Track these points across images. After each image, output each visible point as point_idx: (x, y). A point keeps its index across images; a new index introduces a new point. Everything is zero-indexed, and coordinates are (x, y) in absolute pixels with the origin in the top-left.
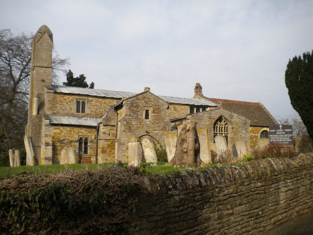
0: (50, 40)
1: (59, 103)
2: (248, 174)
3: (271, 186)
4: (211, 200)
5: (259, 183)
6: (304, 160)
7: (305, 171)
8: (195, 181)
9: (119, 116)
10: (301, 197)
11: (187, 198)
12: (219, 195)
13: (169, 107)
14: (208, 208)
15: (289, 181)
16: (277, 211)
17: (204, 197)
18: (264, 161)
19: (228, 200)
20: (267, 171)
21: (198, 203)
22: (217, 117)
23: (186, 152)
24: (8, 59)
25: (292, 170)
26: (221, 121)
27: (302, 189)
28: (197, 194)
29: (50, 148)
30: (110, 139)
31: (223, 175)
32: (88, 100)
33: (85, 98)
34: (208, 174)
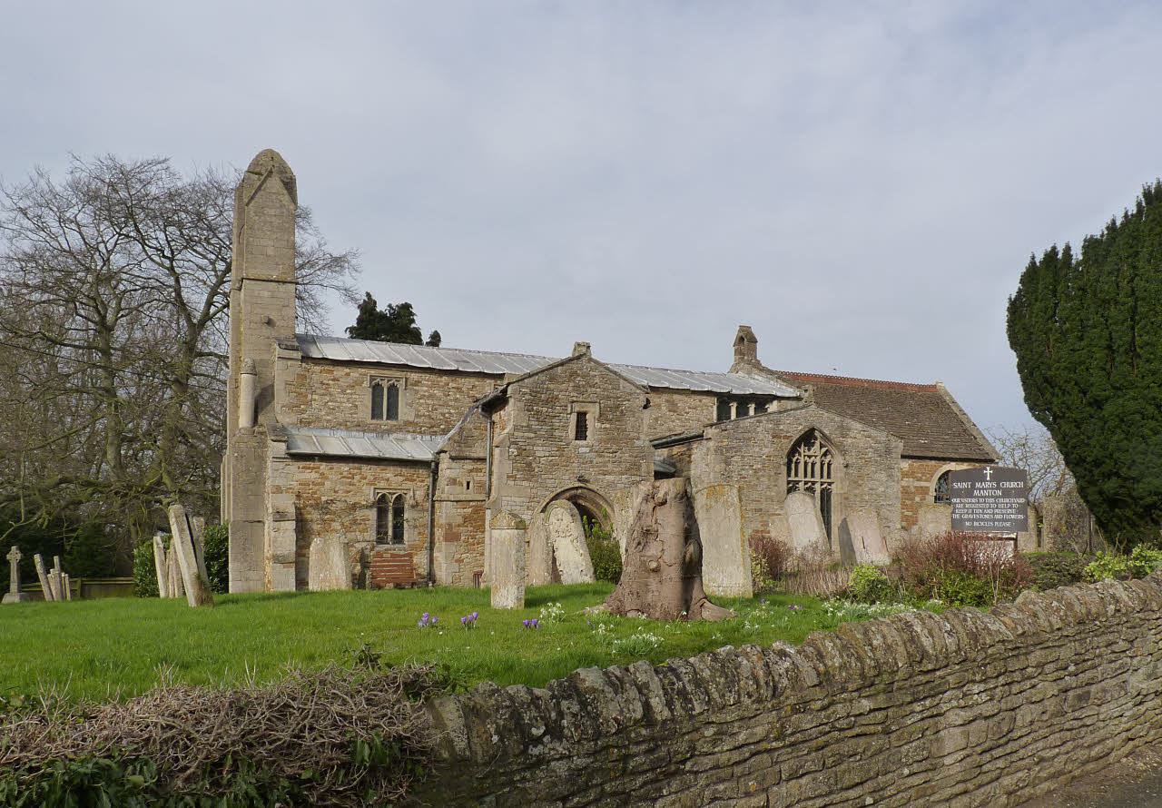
0: (287, 198)
1: (318, 391)
2: (827, 673)
3: (908, 709)
4: (688, 766)
5: (864, 702)
6: (1035, 615)
7: (1038, 653)
8: (631, 707)
9: (497, 430)
10: (1025, 739)
11: (597, 765)
12: (716, 750)
13: (648, 401)
14: (676, 793)
15: (976, 688)
16: (929, 791)
17: (661, 759)
18: (887, 625)
19: (747, 765)
20: (895, 659)
21: (640, 780)
22: (797, 431)
23: (656, 571)
24: (167, 253)
25: (990, 651)
26: (809, 445)
27: (1026, 715)
28: (634, 749)
29: (291, 525)
30: (470, 499)
31: (732, 681)
32: (406, 381)
33: (398, 374)
34: (679, 679)
